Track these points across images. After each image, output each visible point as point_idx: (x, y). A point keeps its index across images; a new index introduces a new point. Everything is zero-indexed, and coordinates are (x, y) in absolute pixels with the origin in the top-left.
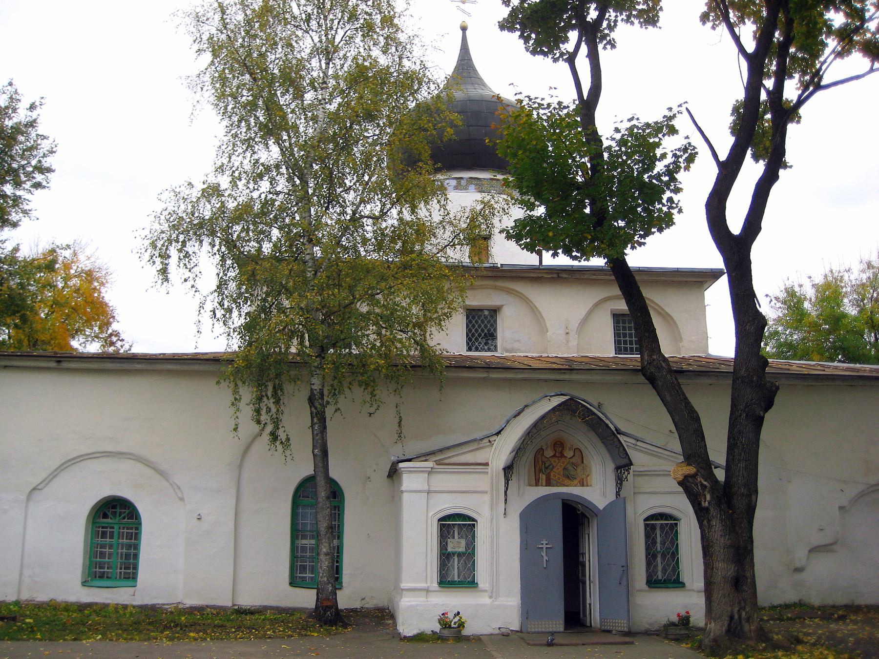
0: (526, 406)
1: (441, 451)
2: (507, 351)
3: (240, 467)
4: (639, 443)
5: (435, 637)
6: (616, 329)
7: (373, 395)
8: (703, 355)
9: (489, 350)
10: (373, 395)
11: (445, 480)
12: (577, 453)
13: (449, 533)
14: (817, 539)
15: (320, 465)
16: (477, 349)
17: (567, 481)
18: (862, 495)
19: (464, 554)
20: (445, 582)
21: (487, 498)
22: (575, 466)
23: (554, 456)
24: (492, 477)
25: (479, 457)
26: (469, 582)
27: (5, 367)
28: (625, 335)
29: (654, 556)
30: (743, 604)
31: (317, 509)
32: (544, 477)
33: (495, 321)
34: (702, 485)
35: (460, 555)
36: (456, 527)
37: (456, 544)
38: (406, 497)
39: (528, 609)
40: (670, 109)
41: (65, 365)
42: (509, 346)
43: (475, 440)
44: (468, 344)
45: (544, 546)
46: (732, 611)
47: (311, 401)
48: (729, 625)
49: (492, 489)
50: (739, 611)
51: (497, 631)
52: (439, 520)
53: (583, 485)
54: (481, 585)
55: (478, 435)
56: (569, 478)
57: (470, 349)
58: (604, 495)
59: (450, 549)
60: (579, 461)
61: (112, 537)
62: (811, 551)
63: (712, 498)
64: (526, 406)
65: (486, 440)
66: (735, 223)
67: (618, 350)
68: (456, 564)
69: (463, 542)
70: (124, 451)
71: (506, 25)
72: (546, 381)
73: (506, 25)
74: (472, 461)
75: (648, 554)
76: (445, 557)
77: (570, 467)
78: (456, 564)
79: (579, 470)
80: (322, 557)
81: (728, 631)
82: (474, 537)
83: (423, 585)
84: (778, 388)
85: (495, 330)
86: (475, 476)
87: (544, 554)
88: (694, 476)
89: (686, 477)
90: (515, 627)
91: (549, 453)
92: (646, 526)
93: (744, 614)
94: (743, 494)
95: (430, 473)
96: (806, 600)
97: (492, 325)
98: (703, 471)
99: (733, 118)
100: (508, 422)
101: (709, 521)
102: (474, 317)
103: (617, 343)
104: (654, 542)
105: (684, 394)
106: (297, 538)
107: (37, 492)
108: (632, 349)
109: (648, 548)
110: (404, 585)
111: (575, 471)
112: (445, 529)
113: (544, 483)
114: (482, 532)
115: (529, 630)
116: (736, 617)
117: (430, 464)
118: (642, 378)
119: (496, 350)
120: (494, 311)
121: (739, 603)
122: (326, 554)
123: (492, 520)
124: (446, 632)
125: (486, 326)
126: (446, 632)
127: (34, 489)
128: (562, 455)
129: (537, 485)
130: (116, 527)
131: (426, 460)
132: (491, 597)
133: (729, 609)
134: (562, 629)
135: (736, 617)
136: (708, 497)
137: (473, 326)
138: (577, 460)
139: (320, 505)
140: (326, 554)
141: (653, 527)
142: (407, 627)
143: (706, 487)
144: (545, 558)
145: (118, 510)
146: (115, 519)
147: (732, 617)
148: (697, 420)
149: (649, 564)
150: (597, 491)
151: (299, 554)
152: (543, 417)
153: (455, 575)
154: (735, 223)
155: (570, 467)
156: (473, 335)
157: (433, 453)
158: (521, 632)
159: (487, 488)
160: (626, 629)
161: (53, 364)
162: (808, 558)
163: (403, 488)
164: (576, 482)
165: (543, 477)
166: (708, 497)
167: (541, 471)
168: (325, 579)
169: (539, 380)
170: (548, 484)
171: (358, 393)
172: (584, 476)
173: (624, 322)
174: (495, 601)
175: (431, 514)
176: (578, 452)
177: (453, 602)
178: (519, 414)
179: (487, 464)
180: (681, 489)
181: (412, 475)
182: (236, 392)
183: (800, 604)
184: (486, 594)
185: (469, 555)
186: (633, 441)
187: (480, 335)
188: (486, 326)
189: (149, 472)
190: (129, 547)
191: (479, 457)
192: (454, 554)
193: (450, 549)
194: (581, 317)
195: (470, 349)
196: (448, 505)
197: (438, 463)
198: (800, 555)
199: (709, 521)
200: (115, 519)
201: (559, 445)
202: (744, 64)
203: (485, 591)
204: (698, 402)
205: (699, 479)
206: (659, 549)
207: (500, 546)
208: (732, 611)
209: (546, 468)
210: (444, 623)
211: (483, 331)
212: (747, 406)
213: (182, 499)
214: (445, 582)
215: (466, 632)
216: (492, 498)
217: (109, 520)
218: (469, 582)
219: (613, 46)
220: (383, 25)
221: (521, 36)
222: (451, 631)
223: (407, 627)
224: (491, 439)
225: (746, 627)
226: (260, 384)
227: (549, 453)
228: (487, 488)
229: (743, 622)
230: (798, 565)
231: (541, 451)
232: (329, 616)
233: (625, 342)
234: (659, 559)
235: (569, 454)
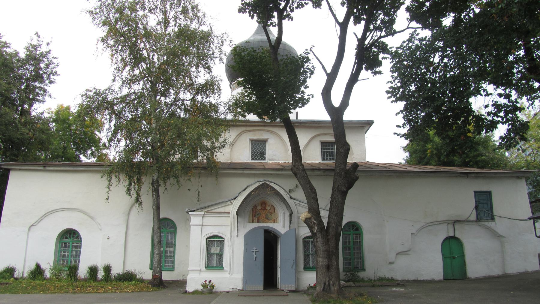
0: (248, 186)
1: (208, 207)
2: (270, 160)
3: (129, 214)
4: (301, 203)
5: (202, 293)
6: (323, 149)
7: (178, 182)
8: (364, 162)
9: (262, 159)
10: (178, 182)
11: (210, 220)
14: (400, 249)
16: (256, 159)
18: (423, 227)
20: (209, 266)
21: (229, 228)
22: (271, 213)
23: (262, 209)
24: (231, 219)
25: (226, 209)
26: (220, 266)
27: (20, 169)
28: (327, 152)
29: (308, 256)
30: (331, 278)
31: (164, 233)
33: (265, 146)
34: (314, 222)
35: (217, 254)
36: (215, 241)
37: (215, 250)
38: (192, 228)
39: (246, 280)
40: (307, 50)
41: (47, 168)
42: (271, 158)
44: (252, 157)
45: (255, 251)
47: (153, 184)
48: (324, 287)
50: (329, 281)
51: (231, 290)
53: (274, 223)
54: (225, 268)
55: (226, 200)
57: (253, 159)
58: (284, 227)
59: (212, 252)
60: (273, 211)
61: (69, 247)
62: (397, 254)
63: (318, 229)
64: (248, 186)
66: (336, 101)
67: (323, 159)
68: (214, 260)
69: (219, 248)
70: (74, 207)
71: (241, 10)
72: (271, 174)
73: (241, 10)
74: (223, 211)
75: (304, 255)
76: (209, 255)
79: (273, 215)
81: (323, 290)
83: (199, 268)
84: (357, 178)
85: (265, 150)
86: (224, 218)
87: (254, 254)
88: (310, 218)
89: (306, 219)
90: (240, 288)
91: (259, 208)
92: (304, 242)
95: (203, 217)
96: (395, 278)
97: (264, 148)
99: (299, 55)
100: (240, 193)
102: (255, 144)
103: (323, 155)
104: (308, 249)
105: (309, 181)
107: (33, 227)
108: (330, 159)
110: (190, 268)
111: (271, 216)
112: (214, 243)
114: (227, 244)
116: (327, 283)
117: (203, 213)
118: (291, 173)
119: (265, 159)
120: (264, 142)
121: (329, 277)
122: (157, 254)
124: (205, 290)
125: (261, 149)
126: (205, 290)
127: (32, 226)
128: (265, 209)
129: (253, 222)
130: (71, 243)
135: (327, 283)
136: (316, 228)
137: (255, 148)
138: (272, 211)
140: (157, 254)
141: (308, 242)
142: (190, 288)
143: (315, 223)
144: (255, 256)
145: (72, 235)
146: (69, 238)
147: (325, 284)
148: (315, 192)
149: (305, 259)
150: (281, 226)
153: (214, 263)
154: (336, 101)
156: (255, 153)
157: (205, 208)
158: (243, 290)
160: (294, 289)
161: (42, 168)
162: (396, 258)
164: (271, 221)
165: (256, 219)
166: (316, 228)
167: (255, 216)
169: (268, 174)
170: (258, 222)
171: (172, 180)
173: (326, 146)
174: (231, 277)
176: (273, 207)
177: (214, 276)
179: (229, 213)
180: (305, 225)
182: (110, 181)
183: (392, 279)
184: (228, 273)
185: (220, 256)
186: (298, 202)
187: (258, 153)
188: (261, 149)
189: (86, 217)
190: (76, 252)
191: (226, 209)
192: (214, 254)
193: (212, 252)
194: (305, 144)
195: (253, 159)
196: (211, 231)
197: (207, 212)
198: (392, 257)
200: (69, 238)
201: (264, 204)
202: (338, 28)
203: (227, 271)
204: (315, 183)
206: (311, 252)
207: (235, 251)
210: (204, 286)
211: (259, 150)
212: (339, 186)
213: (101, 230)
214: (209, 266)
216: (231, 228)
217: (68, 240)
218: (220, 266)
219: (292, 20)
220: (190, 11)
221: (250, 15)
222: (209, 289)
223: (190, 288)
224: (232, 201)
225: (332, 288)
226: (130, 178)
227: (259, 208)
228: (229, 224)
229: (331, 286)
230: (391, 261)
231: (255, 207)
232: (158, 283)
233: (327, 156)
234: (311, 256)
235: (268, 208)
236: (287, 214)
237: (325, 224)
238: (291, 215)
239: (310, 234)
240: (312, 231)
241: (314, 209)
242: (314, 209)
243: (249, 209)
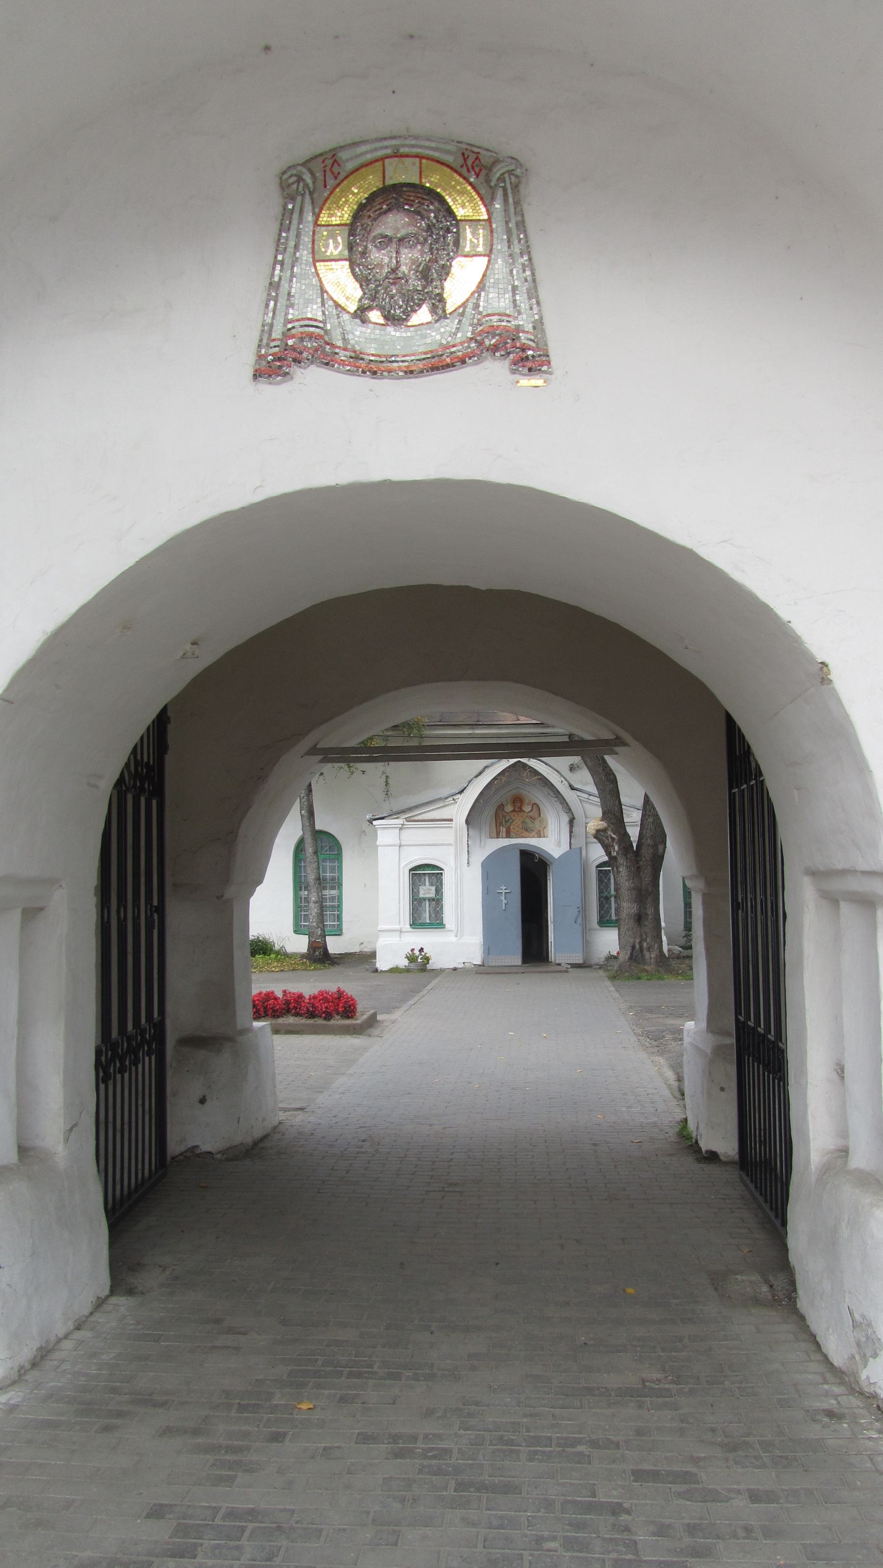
1: (410, 809)
4: (591, 798)
5: (407, 970)
11: (415, 835)
12: (535, 807)
13: (420, 881)
15: (307, 824)
17: (525, 833)
19: (433, 900)
20: (416, 923)
21: (452, 849)
23: (514, 811)
26: (437, 922)
30: (644, 936)
32: (504, 829)
35: (431, 900)
36: (425, 875)
37: (427, 891)
39: (489, 948)
43: (440, 799)
45: (504, 891)
46: (634, 942)
48: (631, 954)
49: (456, 842)
51: (461, 966)
52: (410, 870)
56: (527, 831)
58: (559, 844)
59: (421, 896)
60: (537, 815)
63: (620, 849)
65: (451, 799)
68: (426, 911)
76: (416, 902)
77: (528, 820)
78: (426, 911)
79: (537, 822)
80: (312, 905)
82: (441, 884)
83: (397, 927)
87: (503, 898)
88: (604, 830)
90: (479, 962)
91: (509, 808)
93: (645, 944)
94: (649, 845)
95: (401, 829)
98: (612, 826)
101: (617, 868)
106: (301, 890)
109: (600, 892)
111: (532, 823)
113: (504, 835)
114: (448, 880)
115: (490, 964)
116: (637, 946)
117: (400, 821)
121: (641, 936)
122: (315, 902)
123: (456, 869)
124: (413, 966)
126: (413, 966)
128: (521, 810)
131: (397, 818)
132: (456, 936)
133: (632, 941)
134: (520, 963)
135: (637, 946)
136: (616, 848)
138: (534, 814)
139: (308, 860)
140: (315, 902)
142: (383, 963)
143: (613, 839)
144: (505, 901)
147: (633, 947)
151: (303, 904)
152: (495, 779)
153: (426, 917)
155: (528, 820)
157: (403, 812)
158: (483, 965)
159: (452, 842)
160: (581, 962)
163: (378, 843)
164: (534, 833)
165: (503, 830)
167: (501, 824)
168: (315, 924)
170: (508, 836)
172: (541, 829)
175: (402, 866)
176: (536, 807)
178: (480, 773)
179: (451, 820)
181: (386, 831)
184: (453, 934)
185: (437, 902)
186: (586, 796)
192: (425, 899)
197: (408, 820)
199: (617, 868)
201: (518, 801)
203: (452, 931)
205: (610, 833)
208: (634, 942)
209: (506, 822)
210: (412, 958)
214: (416, 923)
215: (429, 967)
216: (456, 849)
218: (437, 922)
224: (455, 797)
225: (647, 955)
227: (509, 808)
228: (452, 842)
231: (501, 807)
235: (527, 808)
236: (565, 819)
237: (635, 845)
238: (571, 822)
239: (606, 858)
240: (608, 853)
241: (613, 813)
242: (613, 813)
243: (489, 812)
